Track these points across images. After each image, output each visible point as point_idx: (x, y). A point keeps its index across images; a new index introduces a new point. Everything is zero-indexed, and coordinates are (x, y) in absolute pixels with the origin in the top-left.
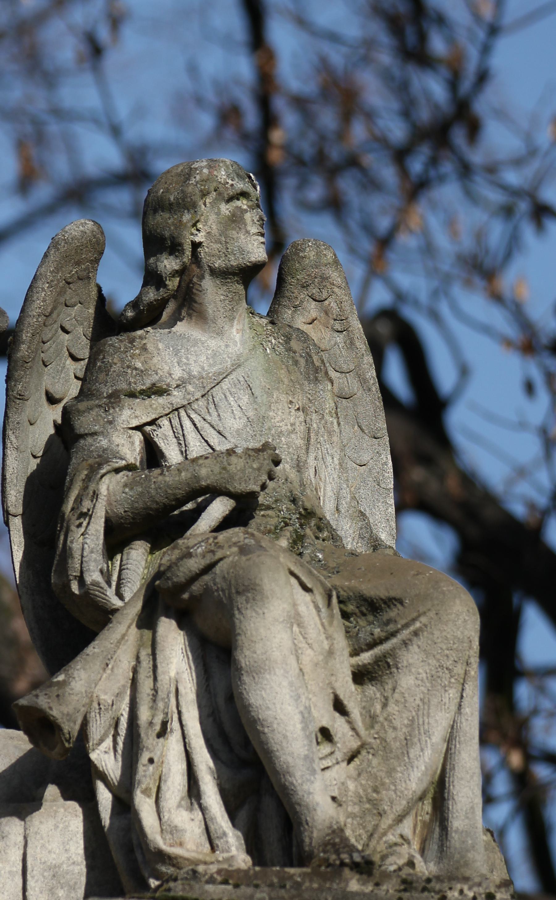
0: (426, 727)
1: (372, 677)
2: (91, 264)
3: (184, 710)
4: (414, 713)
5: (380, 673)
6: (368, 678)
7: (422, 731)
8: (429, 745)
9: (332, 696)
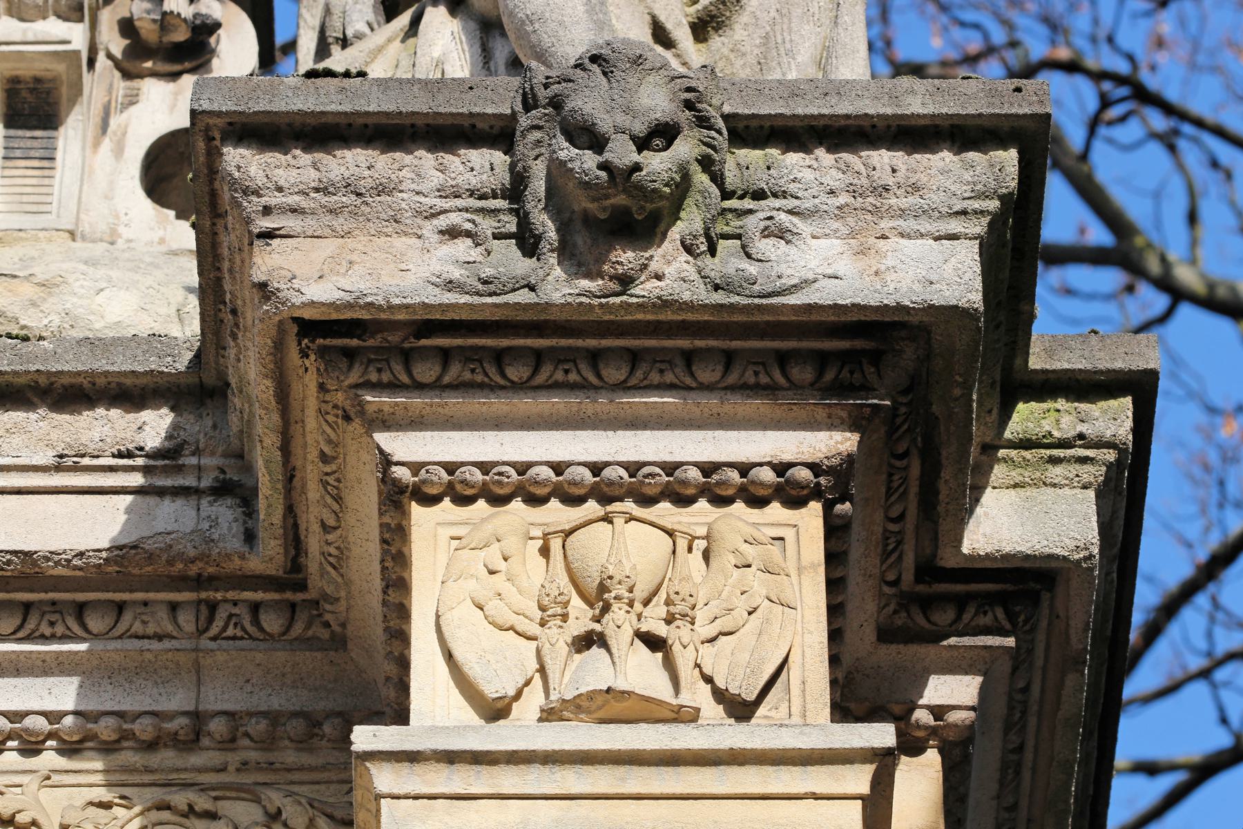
0: (788, 46)
1: (718, 23)
2: (622, 177)
3: (795, 553)
4: (768, 28)
5: (728, 14)
6: (713, 28)
7: (782, 51)
8: (793, 67)
9: (648, 18)
